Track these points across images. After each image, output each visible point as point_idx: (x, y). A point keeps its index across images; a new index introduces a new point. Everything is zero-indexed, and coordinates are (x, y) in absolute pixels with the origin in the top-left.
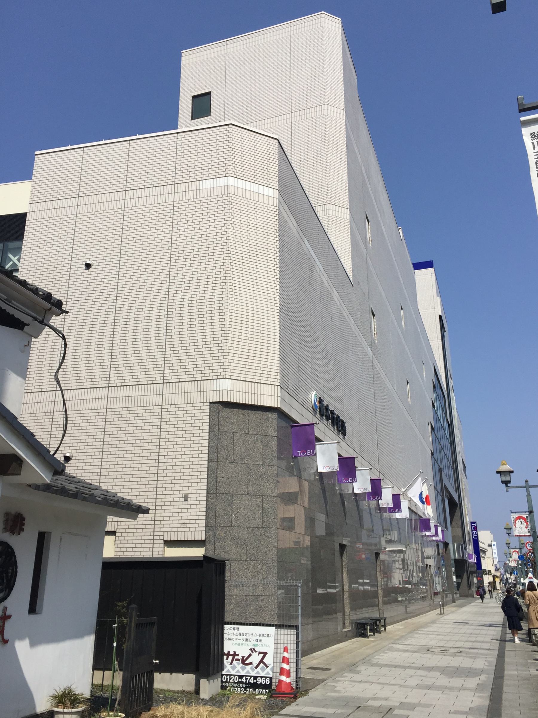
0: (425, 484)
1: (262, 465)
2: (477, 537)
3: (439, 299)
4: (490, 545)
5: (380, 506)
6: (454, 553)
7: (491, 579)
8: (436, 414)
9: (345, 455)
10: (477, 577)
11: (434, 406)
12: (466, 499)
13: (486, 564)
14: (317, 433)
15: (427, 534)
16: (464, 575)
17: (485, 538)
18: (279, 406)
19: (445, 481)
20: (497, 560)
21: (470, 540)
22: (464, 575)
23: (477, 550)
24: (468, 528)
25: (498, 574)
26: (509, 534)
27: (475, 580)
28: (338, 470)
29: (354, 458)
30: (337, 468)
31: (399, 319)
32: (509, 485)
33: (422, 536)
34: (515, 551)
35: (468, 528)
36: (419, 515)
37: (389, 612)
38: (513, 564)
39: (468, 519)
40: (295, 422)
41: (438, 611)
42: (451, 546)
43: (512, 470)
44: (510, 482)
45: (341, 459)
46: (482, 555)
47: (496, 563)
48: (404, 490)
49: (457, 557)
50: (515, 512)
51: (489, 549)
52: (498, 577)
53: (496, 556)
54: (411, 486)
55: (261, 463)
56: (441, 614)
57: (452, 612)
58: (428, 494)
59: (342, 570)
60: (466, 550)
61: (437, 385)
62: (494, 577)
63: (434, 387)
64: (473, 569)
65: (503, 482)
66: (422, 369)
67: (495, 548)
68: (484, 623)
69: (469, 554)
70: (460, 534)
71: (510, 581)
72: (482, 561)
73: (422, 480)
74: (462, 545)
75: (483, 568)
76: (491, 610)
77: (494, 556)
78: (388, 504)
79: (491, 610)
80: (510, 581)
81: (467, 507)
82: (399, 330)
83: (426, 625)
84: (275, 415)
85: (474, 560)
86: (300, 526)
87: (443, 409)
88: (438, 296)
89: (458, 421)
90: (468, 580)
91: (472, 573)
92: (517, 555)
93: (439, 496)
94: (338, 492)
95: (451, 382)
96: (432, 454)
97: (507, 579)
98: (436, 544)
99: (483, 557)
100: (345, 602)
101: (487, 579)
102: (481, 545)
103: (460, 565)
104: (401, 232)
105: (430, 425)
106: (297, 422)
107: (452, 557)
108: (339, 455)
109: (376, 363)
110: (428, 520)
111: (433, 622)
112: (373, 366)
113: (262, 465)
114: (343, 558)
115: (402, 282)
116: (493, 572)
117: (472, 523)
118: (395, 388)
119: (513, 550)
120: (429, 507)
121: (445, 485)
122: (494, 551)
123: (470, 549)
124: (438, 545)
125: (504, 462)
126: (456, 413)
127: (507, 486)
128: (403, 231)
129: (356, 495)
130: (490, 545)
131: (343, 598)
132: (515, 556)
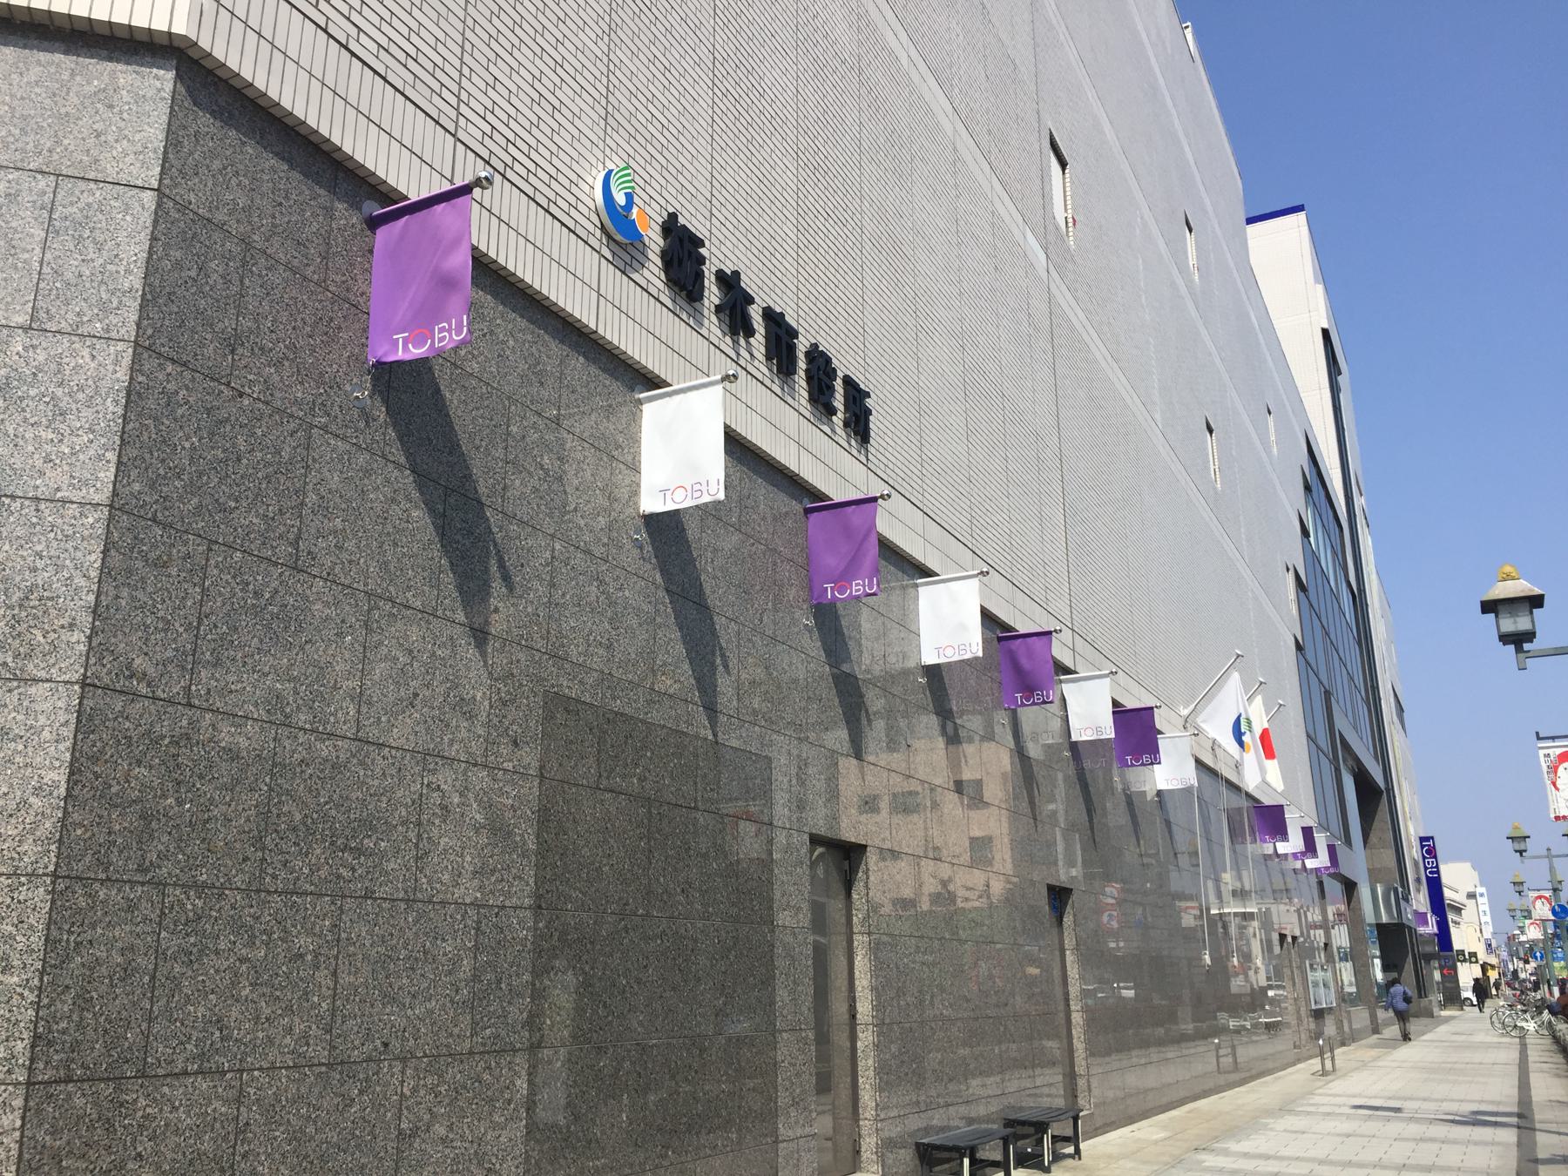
0: (1259, 699)
1: (26, 329)
2: (1438, 872)
3: (1320, 288)
4: (1471, 896)
5: (1074, 738)
6: (1372, 906)
7: (1478, 973)
8: (1312, 557)
9: (1130, 704)
10: (1441, 968)
11: (1305, 533)
12: (1405, 785)
13: (1464, 937)
14: (1060, 652)
15: (1282, 848)
16: (1410, 965)
17: (1457, 878)
18: (180, 28)
19: (1341, 724)
20: (1491, 929)
21: (1418, 880)
22: (1410, 965)
23: (1438, 904)
24: (1413, 852)
25: (1493, 960)
26: (1521, 852)
27: (1437, 976)
28: (980, 654)
29: (1151, 708)
30: (1110, 733)
31: (1179, 255)
32: (1526, 646)
33: (1267, 857)
34: (1540, 897)
35: (1413, 852)
36: (1248, 795)
37: (1103, 1082)
38: (1534, 933)
39: (1411, 831)
40: (817, 495)
41: (1315, 1064)
42: (1364, 892)
43: (1537, 591)
44: (1530, 636)
45: (1119, 711)
46: (1451, 916)
47: (1488, 934)
48: (1185, 712)
49: (1385, 919)
50: (1553, 738)
51: (1470, 903)
52: (1493, 967)
53: (1487, 918)
54: (1208, 696)
55: (21, 319)
56: (1324, 1073)
57: (1364, 1065)
58: (1266, 725)
59: (850, 942)
60: (1407, 900)
61: (1314, 483)
62: (1484, 967)
63: (1307, 488)
64: (1428, 949)
65: (1505, 638)
66: (1267, 428)
67: (1483, 902)
68: (1454, 1107)
69: (1416, 913)
70: (1393, 863)
71: (1522, 976)
72: (1453, 930)
73: (1246, 685)
74: (1396, 890)
75: (1456, 946)
76: (1478, 1057)
77: (1483, 919)
78: (1098, 730)
79: (1478, 1057)
80: (1522, 976)
81: (1406, 799)
82: (1264, 455)
83: (1235, 1130)
84: (160, 81)
85: (1431, 928)
86: (1003, 857)
87: (1334, 552)
88: (1317, 281)
89: (1382, 607)
90: (1416, 971)
91: (1428, 958)
92: (1547, 906)
93: (1325, 763)
94: (1120, 787)
95: (1359, 502)
96: (1299, 647)
97: (1515, 972)
98: (1313, 880)
99: (1456, 923)
100: (861, 1064)
101: (1467, 975)
102: (1447, 893)
103: (1394, 940)
104: (1190, 37)
105: (1292, 571)
106: (825, 497)
107: (1370, 918)
108: (1115, 703)
109: (1063, 298)
110: (1279, 809)
111: (1285, 1108)
112: (1050, 299)
113: (26, 329)
114: (855, 896)
115: (1192, 162)
116: (1483, 956)
117: (1422, 839)
118: (1158, 416)
119: (1536, 894)
120: (1272, 766)
121: (1341, 735)
122: (1481, 908)
123: (1420, 900)
124: (1321, 884)
125: (1508, 569)
126: (1374, 577)
127: (1519, 649)
128: (1196, 33)
129: (1074, 747)
130: (1471, 896)
131: (854, 1049)
132: (1543, 910)
